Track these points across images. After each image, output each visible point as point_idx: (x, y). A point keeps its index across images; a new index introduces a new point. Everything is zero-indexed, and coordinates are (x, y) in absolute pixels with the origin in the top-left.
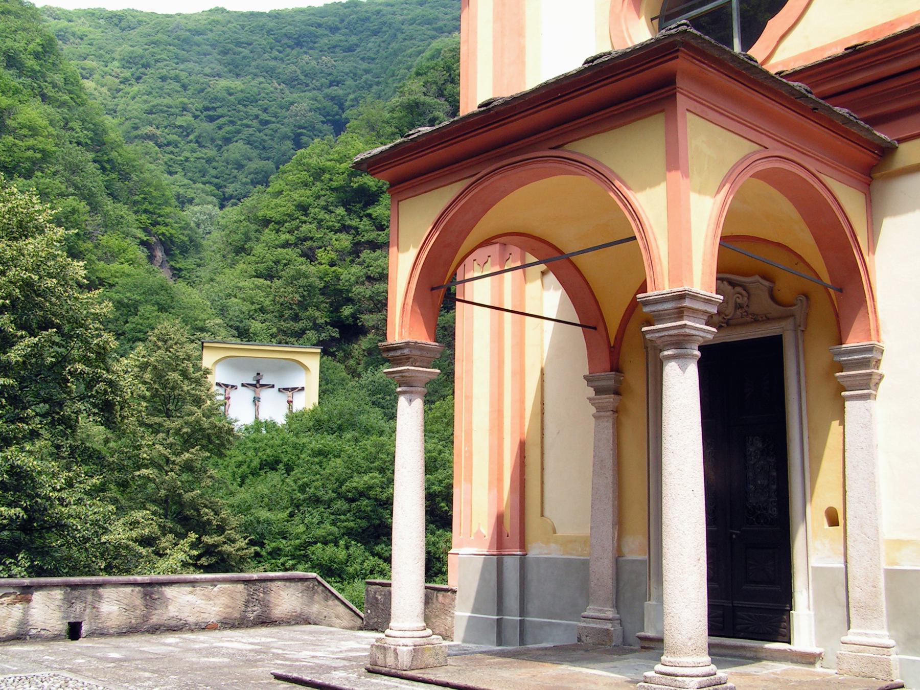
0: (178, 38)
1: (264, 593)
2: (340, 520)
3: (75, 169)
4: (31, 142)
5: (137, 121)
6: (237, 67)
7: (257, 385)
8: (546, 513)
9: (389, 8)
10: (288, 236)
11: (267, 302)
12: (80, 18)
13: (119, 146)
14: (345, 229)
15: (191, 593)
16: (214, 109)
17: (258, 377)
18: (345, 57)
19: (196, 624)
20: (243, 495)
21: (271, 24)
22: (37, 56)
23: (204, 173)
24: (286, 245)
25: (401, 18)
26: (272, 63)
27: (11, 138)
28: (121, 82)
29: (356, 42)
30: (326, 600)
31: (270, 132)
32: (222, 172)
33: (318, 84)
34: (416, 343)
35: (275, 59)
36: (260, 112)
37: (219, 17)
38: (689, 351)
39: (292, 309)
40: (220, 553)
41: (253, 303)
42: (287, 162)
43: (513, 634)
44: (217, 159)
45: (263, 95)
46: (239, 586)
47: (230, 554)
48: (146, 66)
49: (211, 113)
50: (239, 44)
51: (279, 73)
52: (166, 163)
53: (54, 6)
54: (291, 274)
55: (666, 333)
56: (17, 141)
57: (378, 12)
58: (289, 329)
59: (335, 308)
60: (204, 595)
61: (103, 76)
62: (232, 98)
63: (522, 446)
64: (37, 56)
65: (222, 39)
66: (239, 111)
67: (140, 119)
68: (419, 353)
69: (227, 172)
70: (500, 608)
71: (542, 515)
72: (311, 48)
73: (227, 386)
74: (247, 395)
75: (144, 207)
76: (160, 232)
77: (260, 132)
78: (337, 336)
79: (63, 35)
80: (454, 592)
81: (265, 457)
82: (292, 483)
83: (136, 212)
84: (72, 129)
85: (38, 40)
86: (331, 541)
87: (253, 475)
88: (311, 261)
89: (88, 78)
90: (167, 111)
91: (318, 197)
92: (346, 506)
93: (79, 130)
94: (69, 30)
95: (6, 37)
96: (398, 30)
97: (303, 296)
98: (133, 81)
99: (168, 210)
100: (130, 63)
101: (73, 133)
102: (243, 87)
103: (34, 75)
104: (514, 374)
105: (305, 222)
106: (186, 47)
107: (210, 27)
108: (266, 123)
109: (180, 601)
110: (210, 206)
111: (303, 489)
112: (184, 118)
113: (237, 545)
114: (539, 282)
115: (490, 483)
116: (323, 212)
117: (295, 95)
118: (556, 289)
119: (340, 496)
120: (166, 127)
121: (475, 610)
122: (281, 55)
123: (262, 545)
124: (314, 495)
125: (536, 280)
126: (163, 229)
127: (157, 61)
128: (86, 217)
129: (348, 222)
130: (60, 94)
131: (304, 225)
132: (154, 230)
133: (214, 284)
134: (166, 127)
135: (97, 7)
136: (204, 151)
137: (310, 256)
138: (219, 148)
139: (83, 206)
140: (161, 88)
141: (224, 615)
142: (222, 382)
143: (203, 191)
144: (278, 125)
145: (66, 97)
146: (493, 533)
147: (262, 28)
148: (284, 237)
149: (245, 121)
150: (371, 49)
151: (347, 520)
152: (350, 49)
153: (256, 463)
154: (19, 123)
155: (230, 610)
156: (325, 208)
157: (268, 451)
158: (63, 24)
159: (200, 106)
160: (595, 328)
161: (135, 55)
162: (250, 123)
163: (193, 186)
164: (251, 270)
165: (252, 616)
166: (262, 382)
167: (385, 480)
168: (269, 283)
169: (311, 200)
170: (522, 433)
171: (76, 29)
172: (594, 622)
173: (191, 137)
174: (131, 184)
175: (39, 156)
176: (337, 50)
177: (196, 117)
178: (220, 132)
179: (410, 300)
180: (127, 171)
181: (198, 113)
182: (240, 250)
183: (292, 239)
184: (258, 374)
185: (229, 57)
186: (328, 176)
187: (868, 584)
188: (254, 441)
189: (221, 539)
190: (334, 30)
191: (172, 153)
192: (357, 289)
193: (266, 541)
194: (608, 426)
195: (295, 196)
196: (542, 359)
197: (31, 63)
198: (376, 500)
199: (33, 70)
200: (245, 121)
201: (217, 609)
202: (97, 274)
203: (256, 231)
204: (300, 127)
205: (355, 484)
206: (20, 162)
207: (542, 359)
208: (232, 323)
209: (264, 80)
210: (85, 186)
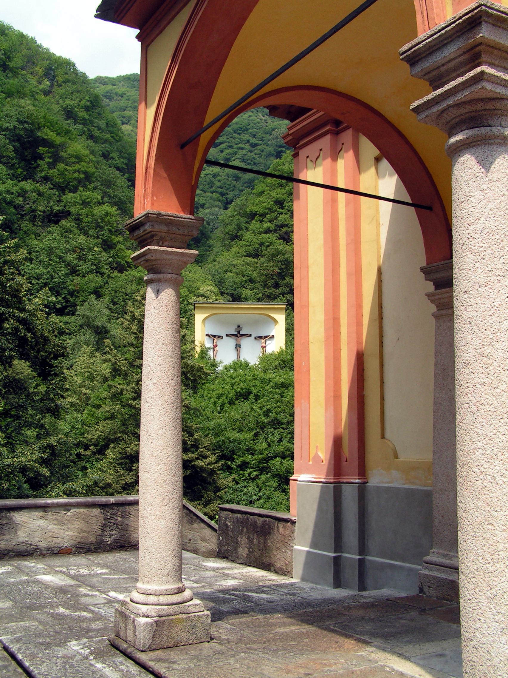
1: (123, 517)
3: (108, 184)
4: (77, 167)
8: (388, 434)
10: (269, 224)
11: (255, 275)
12: (120, 82)
15: (42, 518)
17: (239, 329)
19: (48, 549)
20: (219, 420)
22: (87, 109)
23: (211, 184)
24: (268, 231)
27: (63, 165)
30: (191, 522)
31: (258, 151)
32: (225, 183)
34: (159, 215)
36: (250, 138)
38: (495, 129)
39: (273, 279)
40: (194, 466)
41: (244, 276)
42: (268, 168)
43: (351, 574)
44: (220, 174)
45: (252, 125)
46: (94, 510)
47: (202, 468)
53: (104, 76)
54: (272, 252)
55: (450, 101)
56: (67, 167)
58: (271, 294)
60: (56, 519)
63: (360, 359)
68: (165, 229)
69: (228, 183)
70: (338, 544)
71: (383, 437)
73: (214, 336)
74: (231, 342)
77: (251, 152)
79: (109, 96)
80: (293, 523)
82: (258, 410)
84: (113, 158)
85: (87, 98)
87: (230, 404)
88: (287, 242)
89: (127, 124)
93: (117, 159)
94: (113, 91)
95: (66, 98)
101: (114, 161)
103: (84, 122)
104: (349, 275)
105: (281, 213)
108: (254, 145)
109: (31, 526)
110: (217, 209)
111: (267, 414)
113: (208, 461)
114: (373, 170)
115: (326, 400)
117: (276, 123)
118: (391, 175)
121: (314, 544)
123: (232, 460)
124: (276, 419)
125: (370, 167)
128: (118, 218)
130: (103, 134)
131: (281, 216)
133: (215, 263)
135: (132, 73)
139: (113, 210)
141: (78, 540)
144: (265, 146)
145: (108, 136)
146: (331, 457)
148: (266, 225)
149: (240, 145)
153: (232, 394)
154: (69, 154)
155: (85, 534)
157: (241, 385)
158: (110, 87)
160: (430, 208)
162: (243, 146)
163: (204, 195)
164: (242, 251)
165: (109, 540)
166: (241, 333)
168: (255, 260)
169: (285, 197)
170: (359, 343)
171: (118, 90)
172: (437, 570)
175: (82, 176)
178: (222, 154)
179: (152, 162)
182: (235, 237)
183: (272, 226)
184: (239, 326)
188: (231, 377)
189: (194, 456)
193: (235, 456)
195: (274, 194)
196: (379, 256)
197: (82, 114)
199: (84, 119)
200: (240, 145)
201: (70, 533)
202: (126, 259)
203: (246, 222)
204: (280, 147)
206: (70, 182)
207: (379, 256)
208: (228, 291)
209: (252, 114)
210: (116, 196)
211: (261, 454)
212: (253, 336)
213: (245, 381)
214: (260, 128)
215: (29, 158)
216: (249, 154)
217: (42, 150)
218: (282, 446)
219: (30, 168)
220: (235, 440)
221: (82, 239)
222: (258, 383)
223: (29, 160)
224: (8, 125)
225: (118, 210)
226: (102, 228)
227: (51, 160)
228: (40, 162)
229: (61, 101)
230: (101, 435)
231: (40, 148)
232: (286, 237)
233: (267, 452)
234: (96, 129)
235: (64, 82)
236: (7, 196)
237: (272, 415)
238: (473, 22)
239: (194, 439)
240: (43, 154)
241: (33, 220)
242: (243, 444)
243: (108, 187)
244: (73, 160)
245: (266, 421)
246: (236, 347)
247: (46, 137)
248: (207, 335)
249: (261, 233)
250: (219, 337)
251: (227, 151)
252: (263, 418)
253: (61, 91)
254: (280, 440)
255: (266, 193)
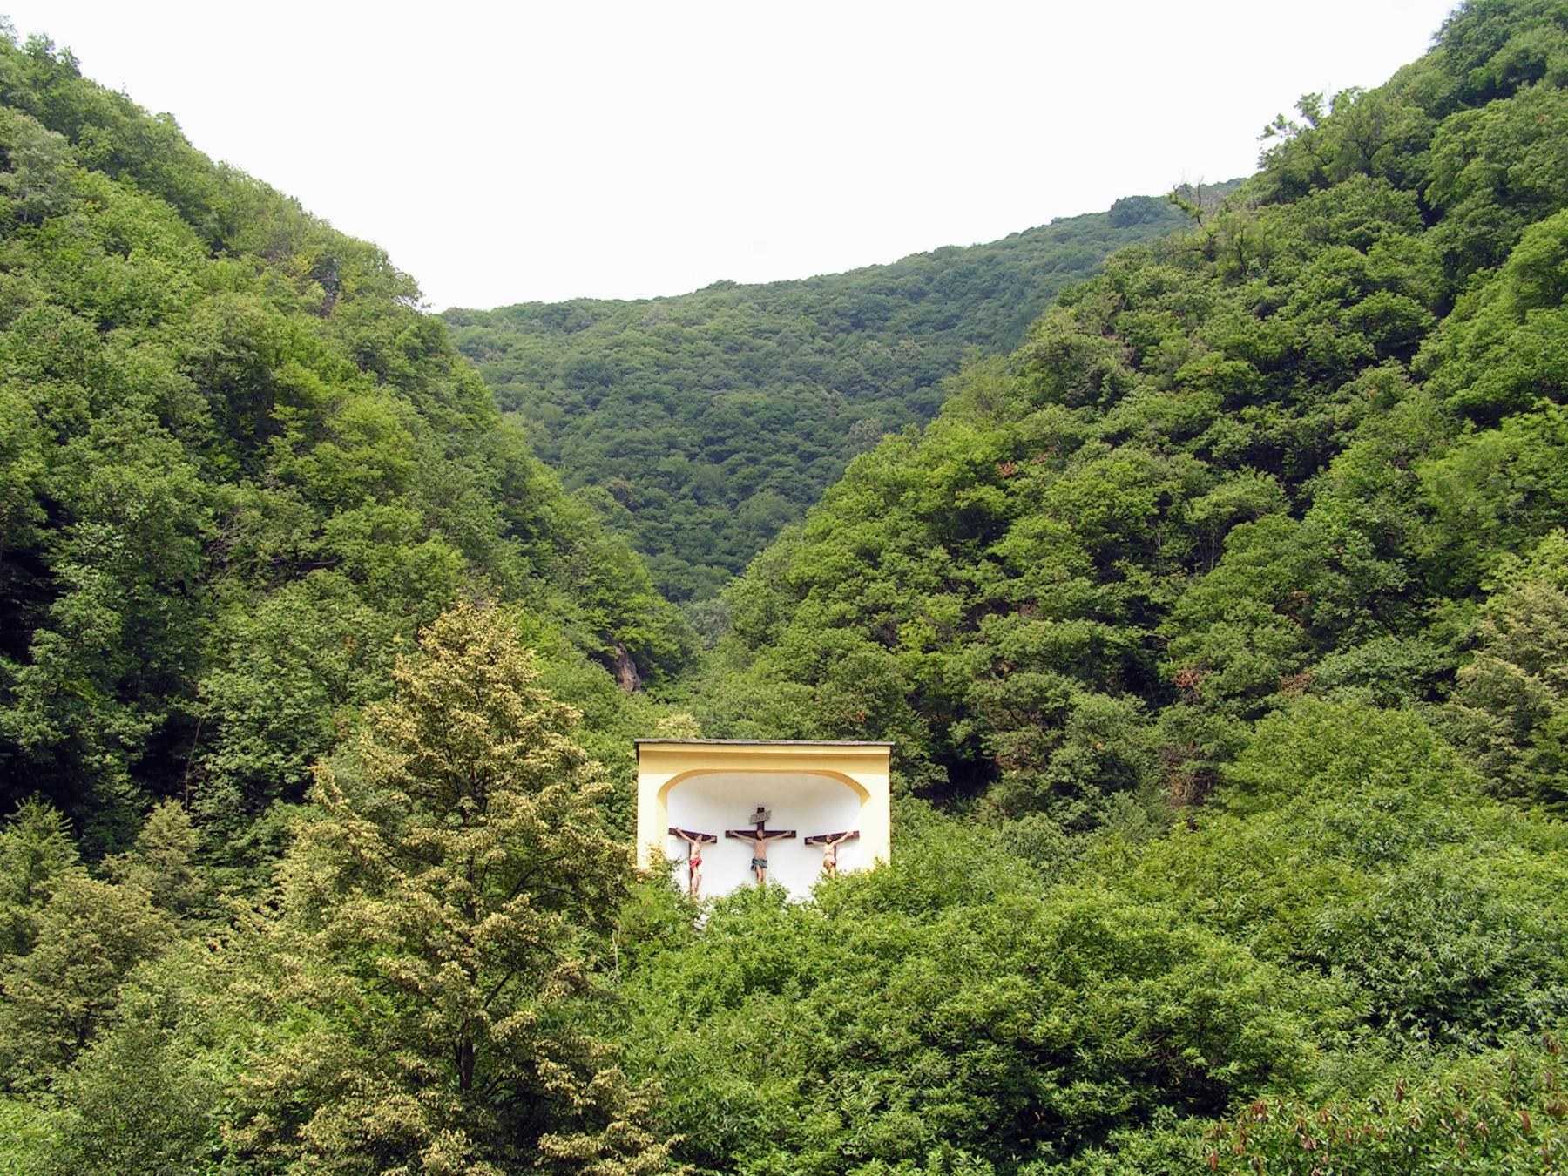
0: (657, 334)
2: (929, 1099)
4: (365, 452)
5: (594, 469)
6: (756, 370)
9: (1008, 252)
13: (555, 496)
14: (950, 585)
16: (722, 440)
18: (938, 337)
21: (810, 298)
24: (841, 622)
25: (1029, 265)
26: (815, 359)
27: (329, 445)
28: (567, 412)
29: (955, 311)
32: (740, 544)
33: (895, 386)
35: (821, 351)
36: (799, 440)
37: (724, 295)
48: (606, 382)
49: (716, 448)
50: (758, 333)
51: (828, 374)
52: (644, 536)
57: (990, 260)
59: (939, 731)
61: (537, 405)
62: (750, 420)
64: (412, 353)
65: (729, 328)
66: (763, 442)
67: (598, 466)
69: (749, 542)
72: (880, 329)
73: (693, 836)
75: (598, 596)
76: (628, 637)
77: (801, 473)
78: (945, 779)
81: (754, 964)
82: (810, 1014)
83: (584, 606)
86: (909, 1153)
90: (643, 451)
91: (896, 533)
92: (943, 1067)
96: (1026, 283)
97: (874, 709)
98: (586, 408)
99: (640, 599)
100: (579, 378)
102: (768, 400)
105: (874, 579)
106: (671, 346)
107: (709, 311)
112: (671, 459)
116: (907, 558)
117: (858, 408)
119: (929, 1041)
120: (642, 476)
122: (830, 345)
124: (867, 1043)
126: (633, 632)
127: (624, 373)
129: (955, 574)
131: (872, 585)
132: (618, 634)
134: (642, 476)
135: (528, 300)
136: (708, 510)
137: (886, 638)
138: (733, 504)
140: (632, 415)
142: (681, 827)
143: (708, 576)
147: (795, 304)
148: (837, 608)
149: (774, 457)
150: (981, 320)
151: (948, 1099)
152: (947, 325)
153: (733, 976)
156: (910, 551)
159: (697, 438)
161: (588, 365)
162: (783, 459)
163: (691, 570)
166: (768, 827)
167: (1038, 993)
168: (810, 688)
173: (685, 490)
174: (574, 559)
176: (924, 327)
177: (692, 457)
178: (734, 478)
180: (568, 536)
181: (696, 450)
182: (762, 640)
184: (761, 810)
185: (741, 357)
186: (911, 494)
190: (917, 296)
191: (653, 517)
192: (977, 688)
195: (854, 534)
197: (399, 362)
198: (1022, 1044)
200: (774, 457)
205: (961, 1007)
211: (821, 1149)
213: (773, 939)
214: (822, 418)
215: (249, 432)
216: (797, 476)
217: (281, 411)
218: (888, 1122)
219: (250, 455)
220: (735, 1108)
221: (365, 614)
222: (812, 943)
223: (248, 438)
224: (199, 349)
225: (464, 556)
226: (420, 595)
227: (301, 436)
228: (274, 440)
229: (349, 332)
230: (290, 1076)
231: (278, 407)
232: (885, 632)
233: (839, 1142)
234: (431, 399)
235: (358, 291)
236: (175, 501)
237: (855, 1030)
239: (595, 1087)
240: (283, 423)
241: (247, 574)
242: (763, 1117)
243: (444, 504)
244: (356, 436)
245: (835, 1048)
247: (291, 381)
248: (673, 832)
249: (824, 626)
250: (706, 838)
251: (746, 471)
252: (827, 1040)
253: (351, 308)
254: (882, 1106)
255: (834, 533)
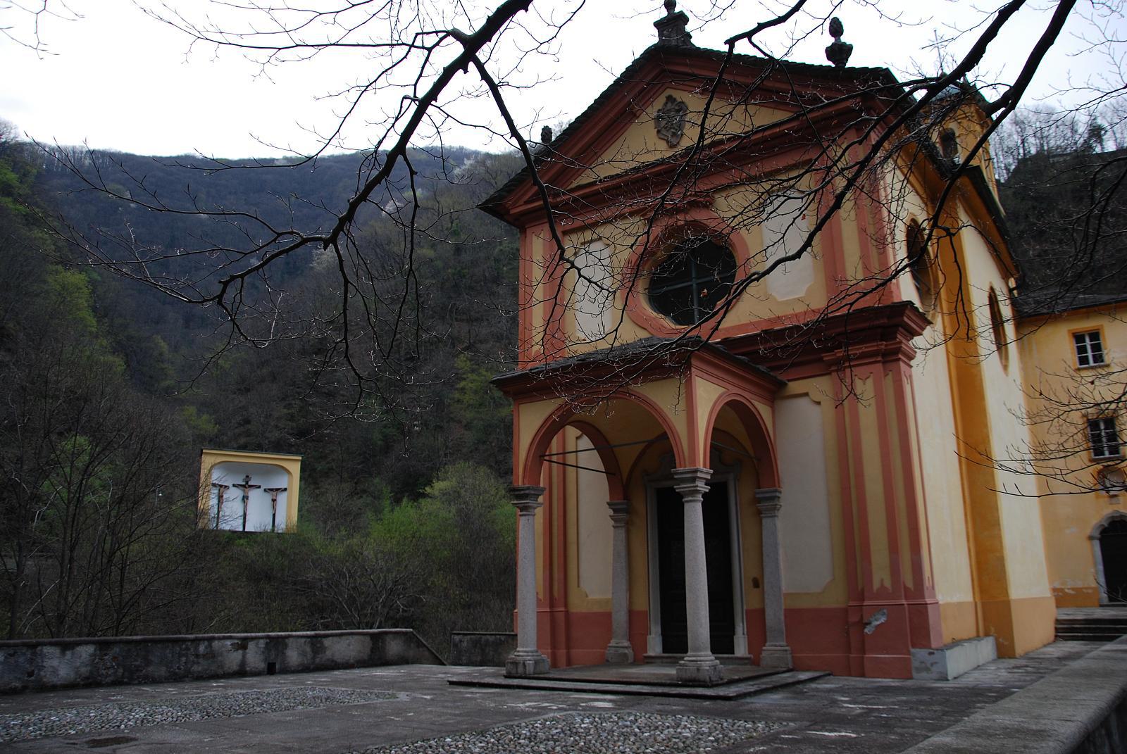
7: (246, 486)
8: (582, 585)
71: (578, 586)
73: (221, 486)
74: (238, 493)
160: (614, 474)
166: (250, 483)
184: (247, 477)
187: (774, 616)
194: (622, 532)
212: (262, 488)
238: (1096, 439)
246: (243, 499)
250: (226, 487)
